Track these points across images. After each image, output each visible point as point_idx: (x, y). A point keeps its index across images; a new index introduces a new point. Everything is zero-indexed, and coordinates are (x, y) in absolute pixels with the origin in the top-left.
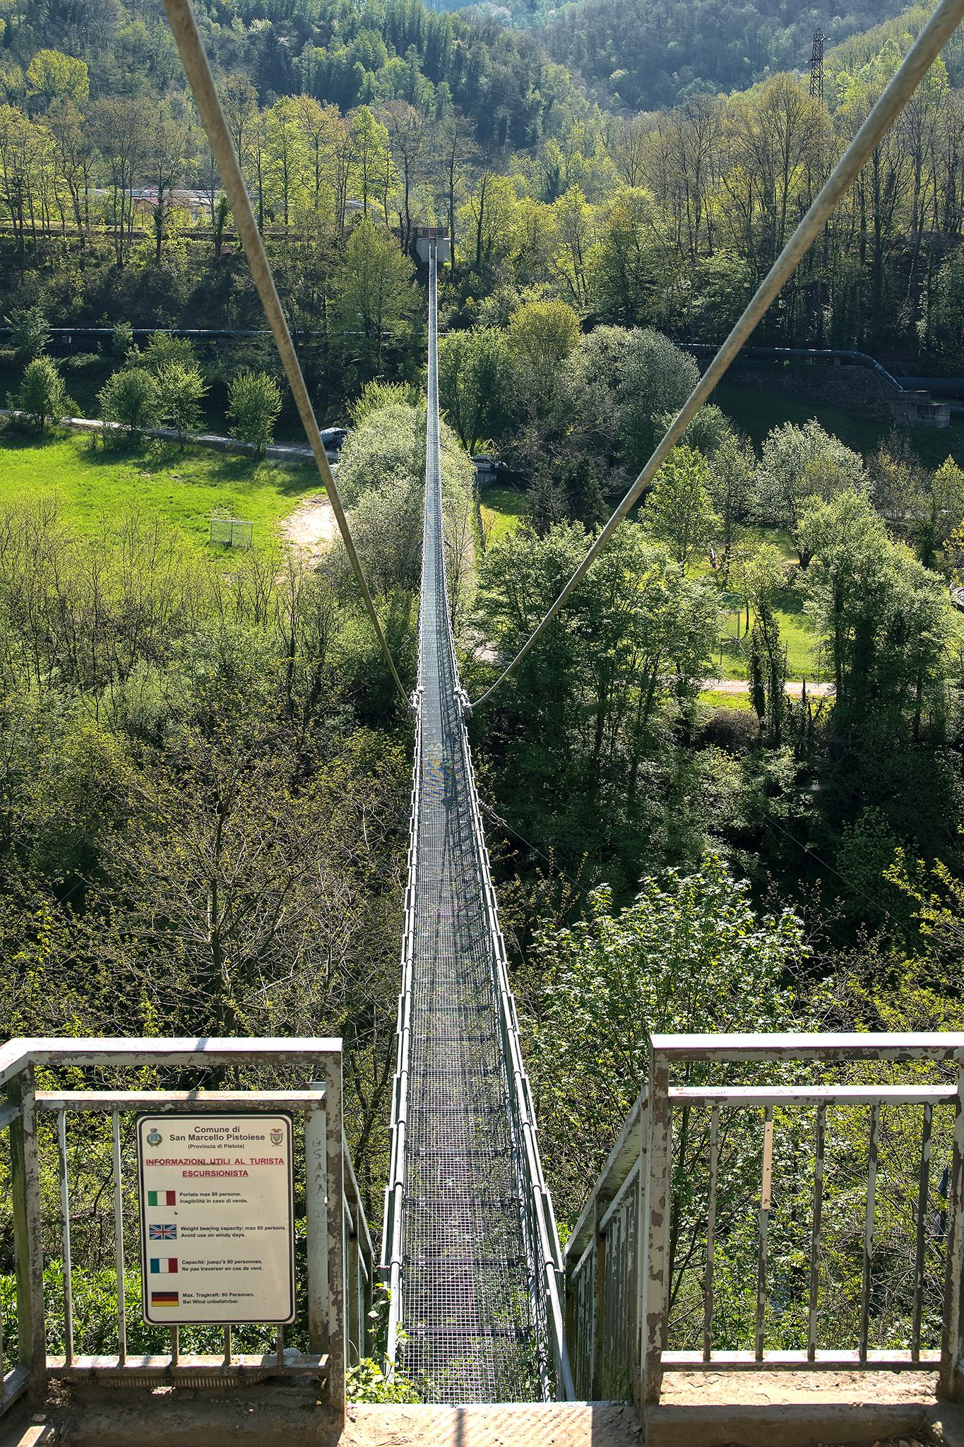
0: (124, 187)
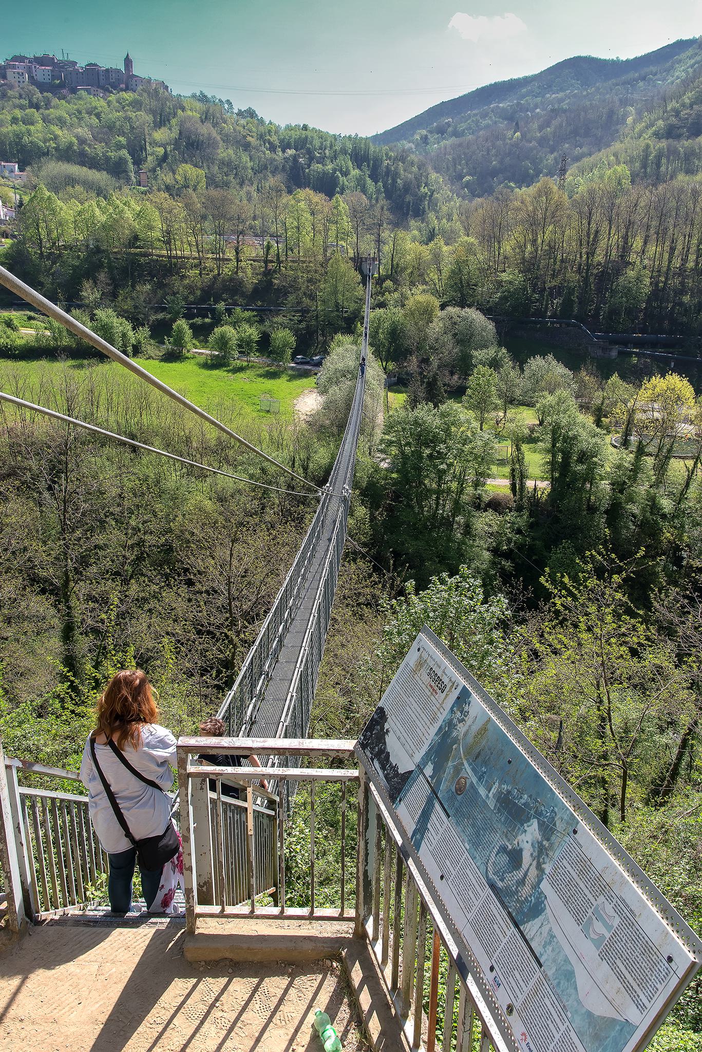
0: (220, 235)
